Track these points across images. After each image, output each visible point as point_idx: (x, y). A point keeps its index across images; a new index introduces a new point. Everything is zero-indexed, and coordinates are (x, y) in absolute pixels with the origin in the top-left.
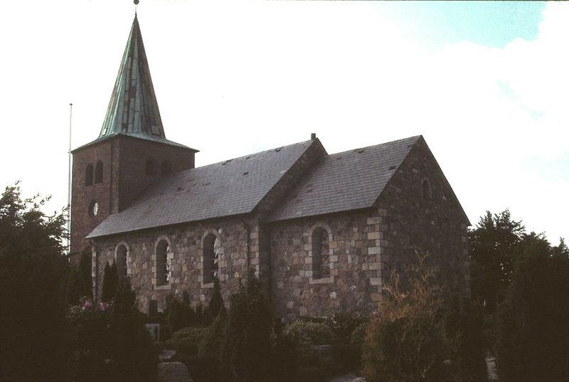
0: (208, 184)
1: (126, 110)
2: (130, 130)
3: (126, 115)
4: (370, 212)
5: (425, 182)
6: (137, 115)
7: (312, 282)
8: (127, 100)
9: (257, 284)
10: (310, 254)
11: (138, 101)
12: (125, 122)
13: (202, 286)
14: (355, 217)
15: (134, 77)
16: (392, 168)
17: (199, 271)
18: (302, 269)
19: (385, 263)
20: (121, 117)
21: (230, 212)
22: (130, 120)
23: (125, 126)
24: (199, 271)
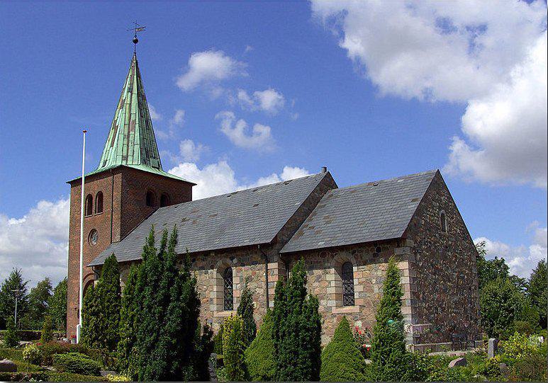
0: (216, 215)
1: (126, 142)
2: (130, 162)
3: (125, 148)
4: (397, 242)
5: (443, 215)
6: (137, 148)
7: (335, 311)
8: (126, 133)
9: (195, 375)
10: (333, 284)
11: (137, 134)
12: (125, 155)
13: (216, 314)
14: (377, 250)
15: (133, 111)
16: (413, 201)
17: (212, 300)
18: (323, 299)
19: (375, 255)
20: (129, 150)
21: (247, 243)
22: (130, 153)
23: (125, 158)
24: (212, 300)
